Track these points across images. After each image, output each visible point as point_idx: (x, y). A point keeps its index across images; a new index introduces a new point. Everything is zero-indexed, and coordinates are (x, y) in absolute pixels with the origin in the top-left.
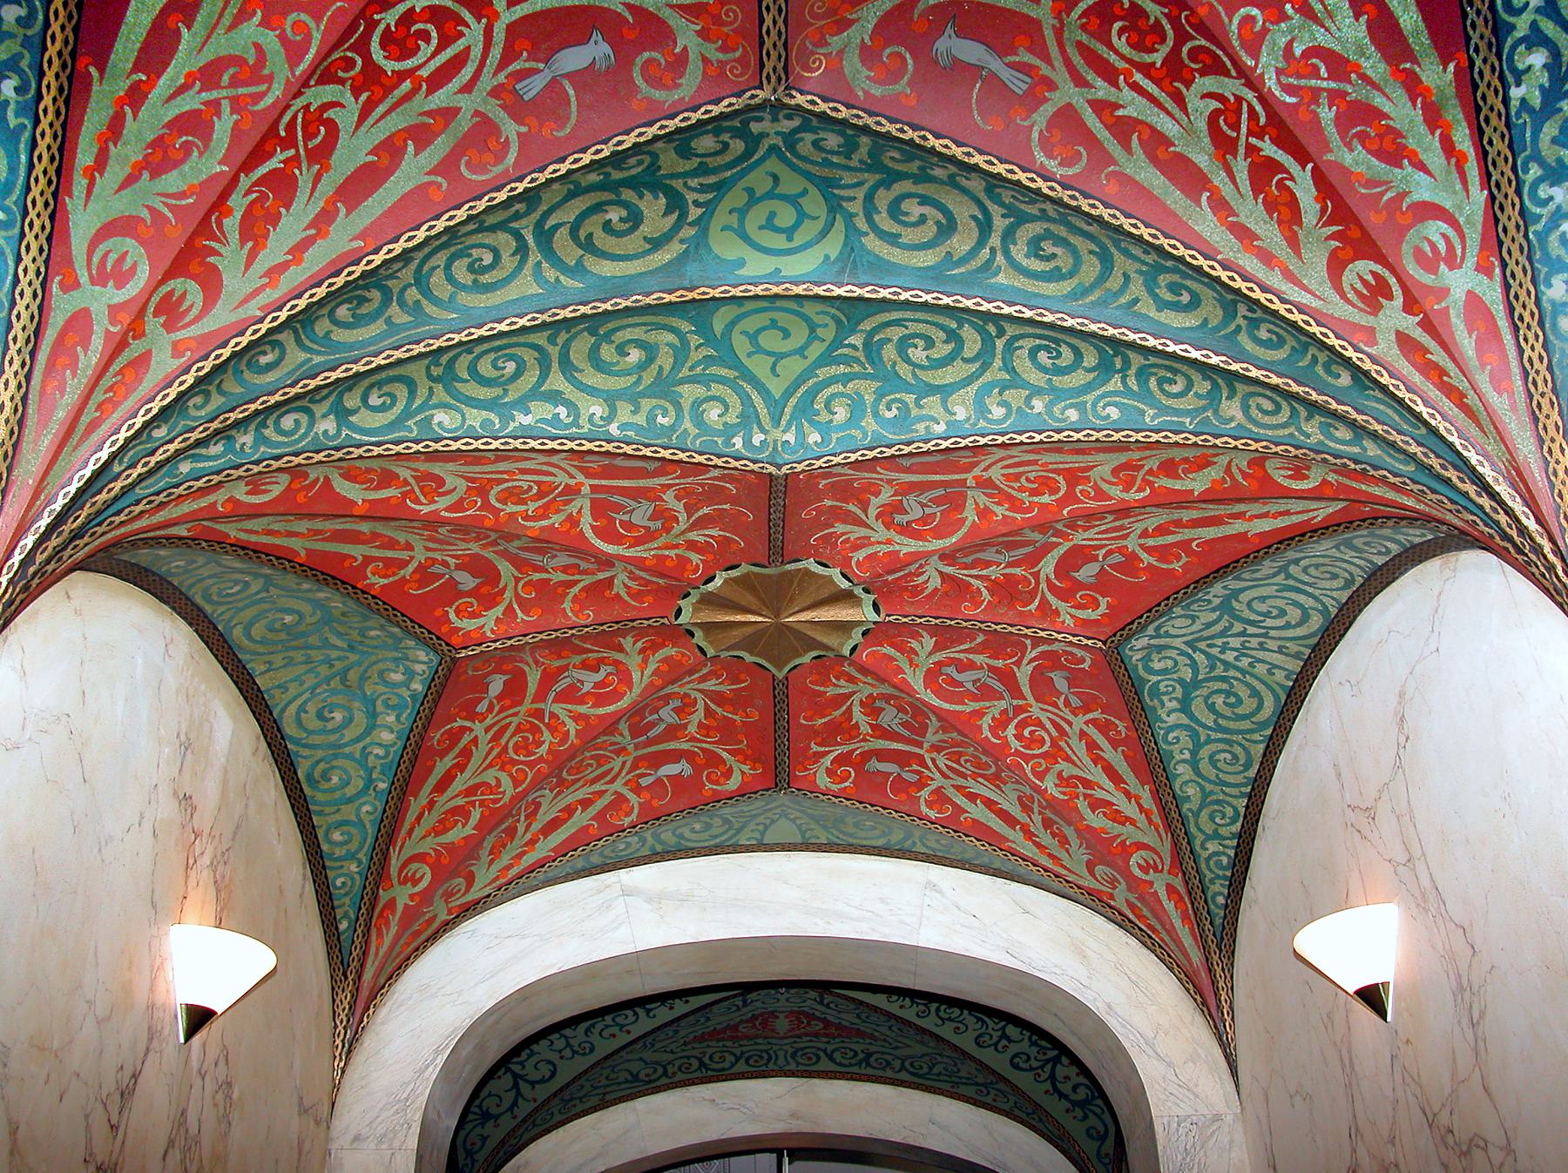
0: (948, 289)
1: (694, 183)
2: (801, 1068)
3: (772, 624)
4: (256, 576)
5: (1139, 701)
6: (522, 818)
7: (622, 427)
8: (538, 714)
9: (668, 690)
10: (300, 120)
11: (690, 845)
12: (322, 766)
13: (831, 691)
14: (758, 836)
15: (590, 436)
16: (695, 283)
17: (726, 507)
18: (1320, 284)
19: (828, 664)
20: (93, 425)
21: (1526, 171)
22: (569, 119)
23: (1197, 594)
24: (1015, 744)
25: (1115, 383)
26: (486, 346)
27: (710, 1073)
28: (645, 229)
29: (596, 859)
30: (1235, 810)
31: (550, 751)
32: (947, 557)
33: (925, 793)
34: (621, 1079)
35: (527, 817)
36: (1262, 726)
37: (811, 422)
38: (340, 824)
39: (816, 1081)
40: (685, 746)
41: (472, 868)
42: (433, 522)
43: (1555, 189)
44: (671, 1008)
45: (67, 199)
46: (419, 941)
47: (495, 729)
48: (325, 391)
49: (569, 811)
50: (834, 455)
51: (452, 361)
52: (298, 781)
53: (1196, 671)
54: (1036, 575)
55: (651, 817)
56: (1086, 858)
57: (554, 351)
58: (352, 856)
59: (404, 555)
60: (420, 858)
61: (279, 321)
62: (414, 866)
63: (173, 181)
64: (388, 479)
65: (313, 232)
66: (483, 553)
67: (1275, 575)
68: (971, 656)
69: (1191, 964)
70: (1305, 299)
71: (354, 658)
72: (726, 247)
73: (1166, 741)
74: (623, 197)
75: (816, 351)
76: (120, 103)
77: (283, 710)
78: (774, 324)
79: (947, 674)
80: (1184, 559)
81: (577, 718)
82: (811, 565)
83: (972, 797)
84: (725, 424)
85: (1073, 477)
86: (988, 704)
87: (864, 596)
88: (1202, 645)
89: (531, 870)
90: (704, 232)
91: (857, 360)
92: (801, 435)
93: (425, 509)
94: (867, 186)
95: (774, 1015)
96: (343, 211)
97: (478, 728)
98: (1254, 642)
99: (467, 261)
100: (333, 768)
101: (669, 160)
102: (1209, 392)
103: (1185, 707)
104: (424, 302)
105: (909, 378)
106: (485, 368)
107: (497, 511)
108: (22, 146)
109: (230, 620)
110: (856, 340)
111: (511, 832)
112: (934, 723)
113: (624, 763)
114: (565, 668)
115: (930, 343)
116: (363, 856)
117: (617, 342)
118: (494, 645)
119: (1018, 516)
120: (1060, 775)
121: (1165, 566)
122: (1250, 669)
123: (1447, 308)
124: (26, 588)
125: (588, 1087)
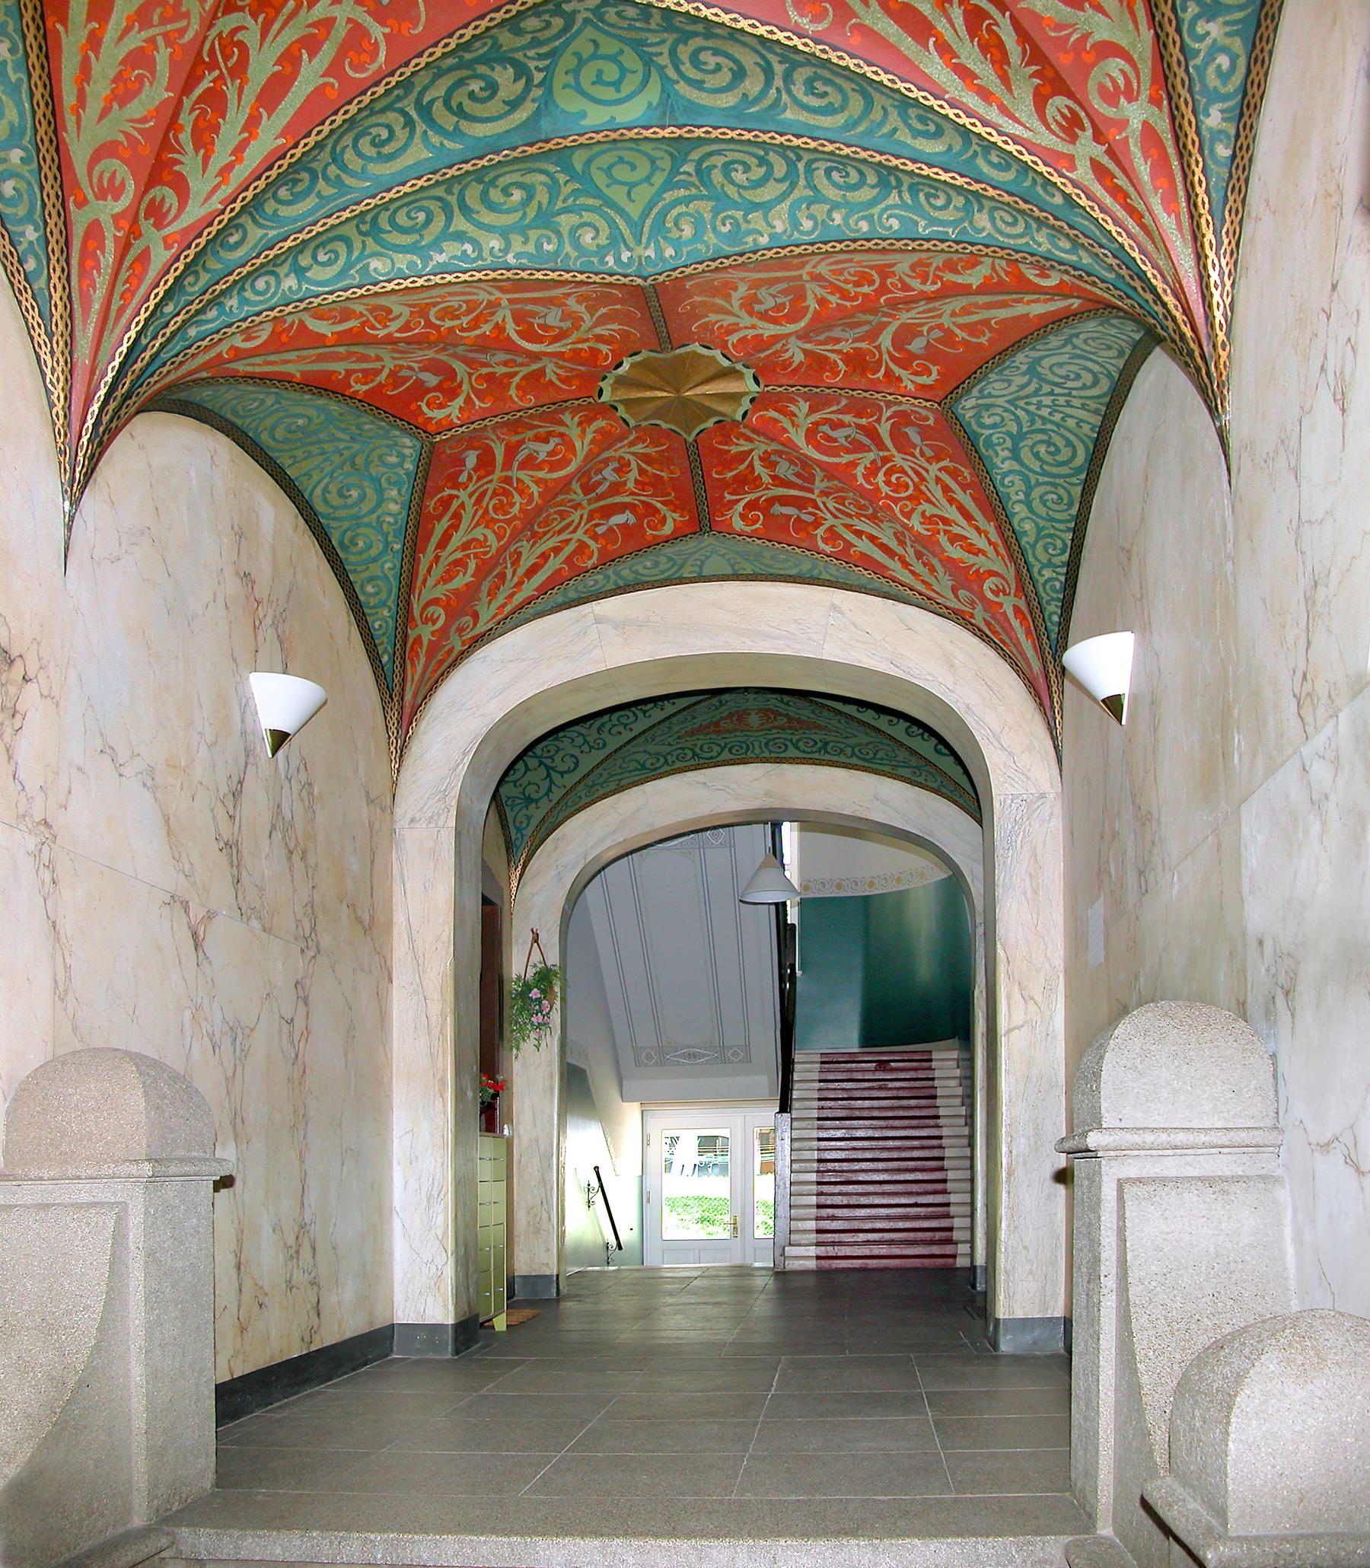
0: (748, 126)
1: (531, 53)
2: (773, 755)
3: (675, 398)
4: (268, 394)
5: (976, 452)
6: (509, 566)
7: (517, 256)
8: (508, 480)
9: (606, 454)
10: (217, 46)
11: (645, 579)
12: (349, 534)
13: (734, 449)
14: (698, 570)
15: (493, 267)
16: (550, 136)
17: (619, 307)
18: (1029, 117)
19: (726, 429)
20: (121, 311)
21: (1185, 9)
22: (419, 19)
23: (1004, 362)
24: (885, 489)
25: (893, 198)
26: (398, 204)
27: (702, 761)
28: (502, 94)
29: (572, 595)
30: (1063, 541)
31: (521, 510)
32: (803, 336)
33: (820, 532)
34: (632, 768)
35: (513, 564)
36: (1077, 471)
37: (665, 238)
38: (371, 580)
39: (785, 766)
40: (628, 499)
41: (477, 608)
42: (390, 340)
43: (1211, 24)
44: (662, 709)
45: (65, 135)
46: (443, 668)
47: (477, 494)
48: (283, 257)
49: (544, 557)
50: (686, 266)
51: (375, 218)
52: (334, 548)
53: (1020, 425)
54: (878, 348)
55: (607, 559)
56: (950, 583)
57: (453, 200)
58: (384, 604)
59: (377, 365)
60: (435, 602)
61: (236, 211)
62: (432, 609)
63: (137, 108)
64: (346, 315)
65: (246, 135)
66: (437, 357)
67: (1063, 346)
68: (840, 416)
69: (1032, 672)
70: (1019, 131)
71: (356, 447)
72: (568, 102)
73: (1003, 485)
74: (478, 71)
75: (659, 179)
76: (84, 49)
77: (311, 494)
78: (621, 160)
79: (824, 433)
80: (988, 335)
81: (538, 482)
82: (696, 347)
83: (858, 533)
84: (598, 246)
85: (884, 272)
86: (859, 456)
87: (745, 370)
88: (1021, 403)
89: (521, 607)
90: (550, 91)
91: (693, 185)
92: (659, 251)
93: (381, 333)
94: (669, 43)
95: (746, 712)
96: (265, 115)
97: (463, 495)
98: (1062, 400)
99: (368, 138)
100: (357, 535)
101: (506, 38)
102: (964, 205)
103: (1015, 455)
104: (343, 176)
105: (736, 197)
106: (402, 219)
107: (437, 328)
108: (24, 95)
109: (257, 428)
110: (689, 168)
111: (502, 577)
112: (819, 474)
113: (582, 516)
114: (521, 443)
115: (747, 169)
116: (391, 603)
117: (501, 186)
118: (461, 430)
119: (848, 304)
120: (923, 513)
121: (975, 340)
122: (1062, 423)
123: (1127, 138)
124: (101, 443)
125: (605, 776)
